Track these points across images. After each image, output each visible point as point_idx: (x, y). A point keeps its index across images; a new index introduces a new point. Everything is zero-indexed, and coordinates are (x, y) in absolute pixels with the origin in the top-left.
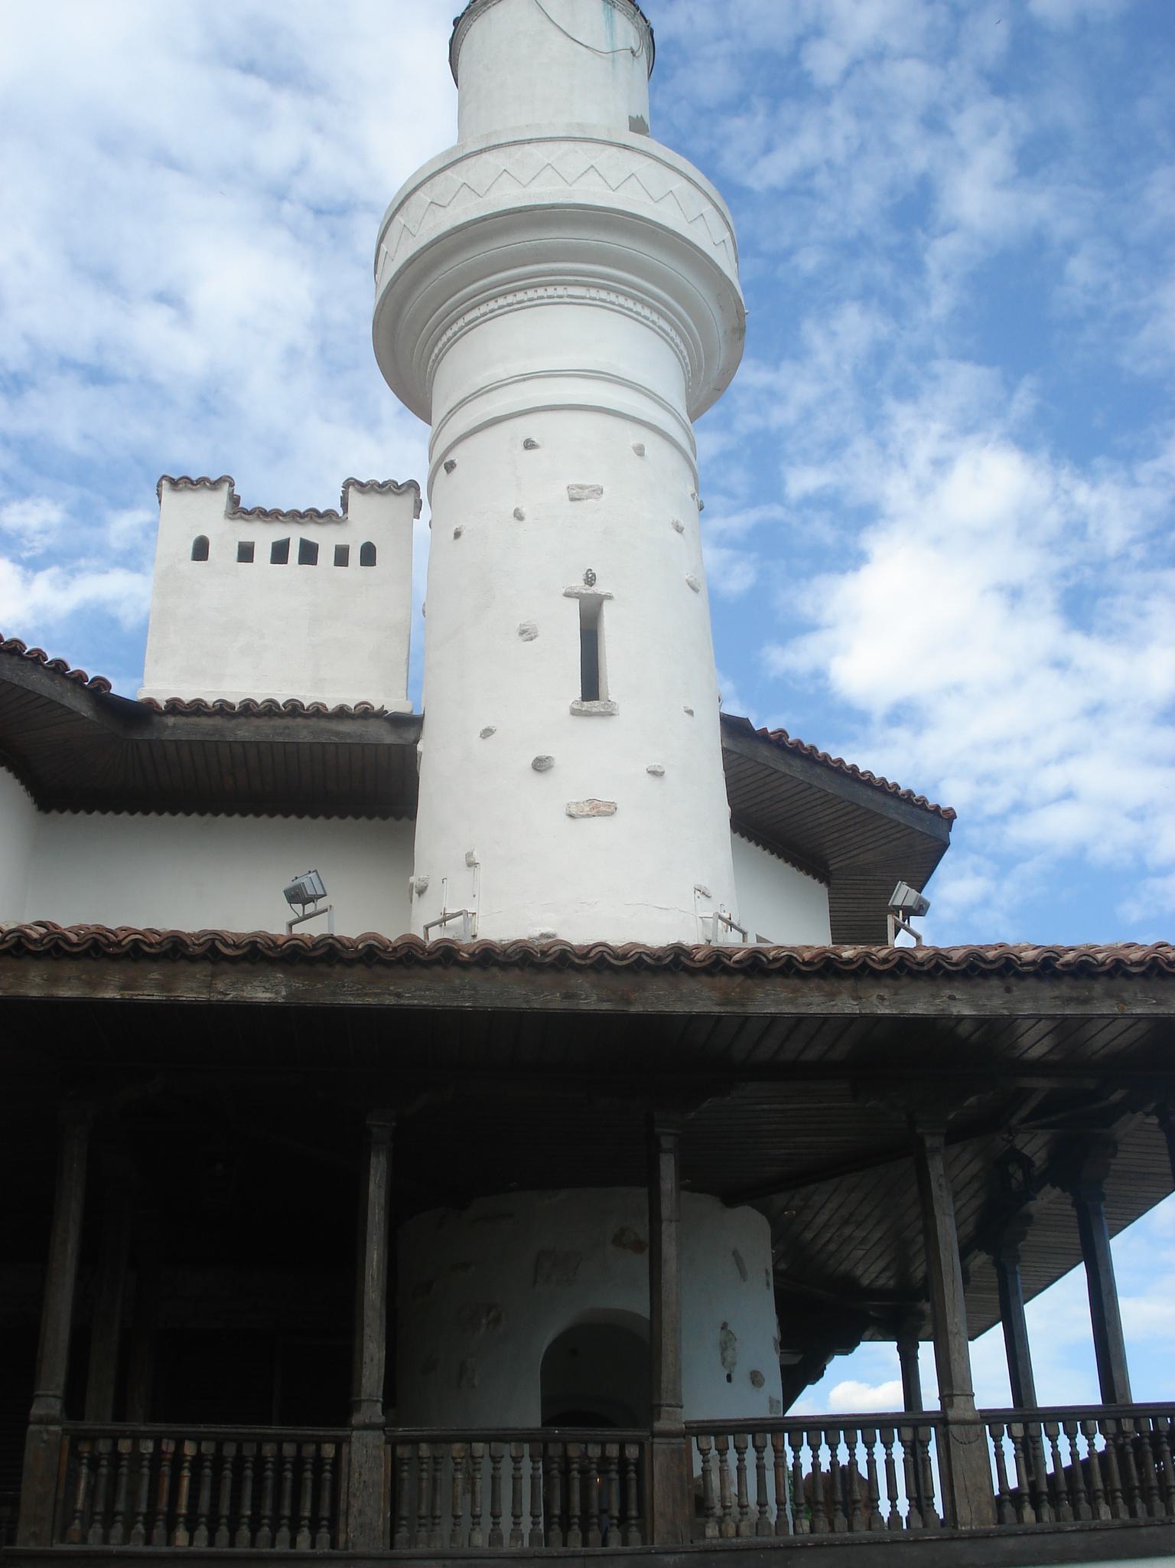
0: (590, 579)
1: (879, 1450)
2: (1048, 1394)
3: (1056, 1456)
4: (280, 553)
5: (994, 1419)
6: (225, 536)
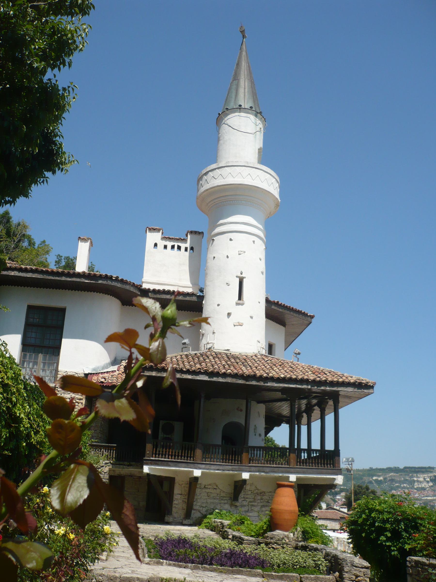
0: (241, 274)
1: (258, 452)
2: (313, 447)
3: (304, 456)
4: (173, 247)
5: (304, 450)
6: (161, 243)
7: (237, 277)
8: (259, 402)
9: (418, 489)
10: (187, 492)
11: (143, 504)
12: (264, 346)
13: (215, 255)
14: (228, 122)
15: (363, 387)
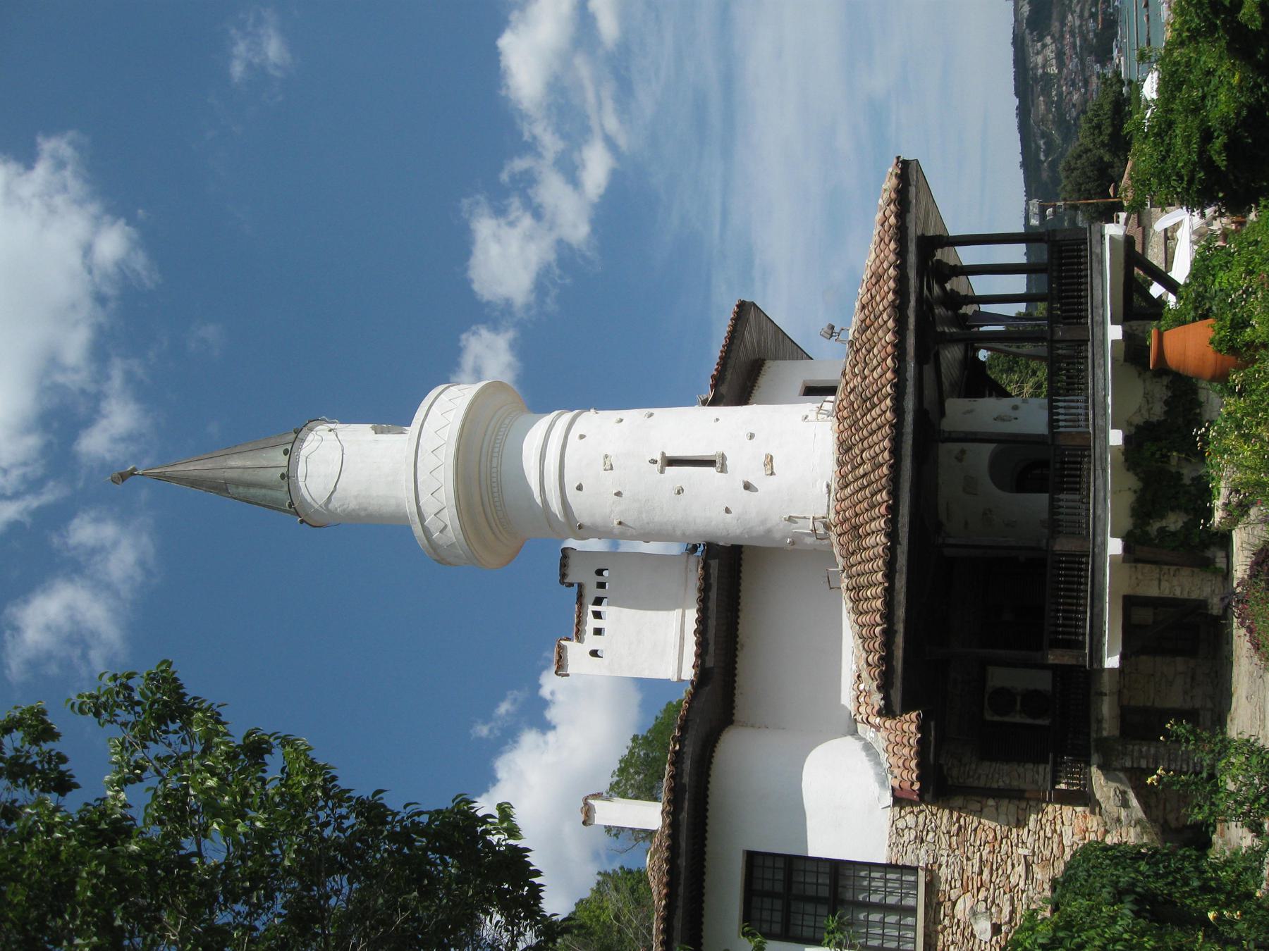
0: (654, 462)
4: (597, 615)
6: (591, 641)
7: (662, 472)
8: (942, 413)
9: (1061, 64)
10: (1153, 567)
11: (1180, 664)
12: (814, 406)
13: (616, 522)
14: (322, 501)
15: (908, 176)
